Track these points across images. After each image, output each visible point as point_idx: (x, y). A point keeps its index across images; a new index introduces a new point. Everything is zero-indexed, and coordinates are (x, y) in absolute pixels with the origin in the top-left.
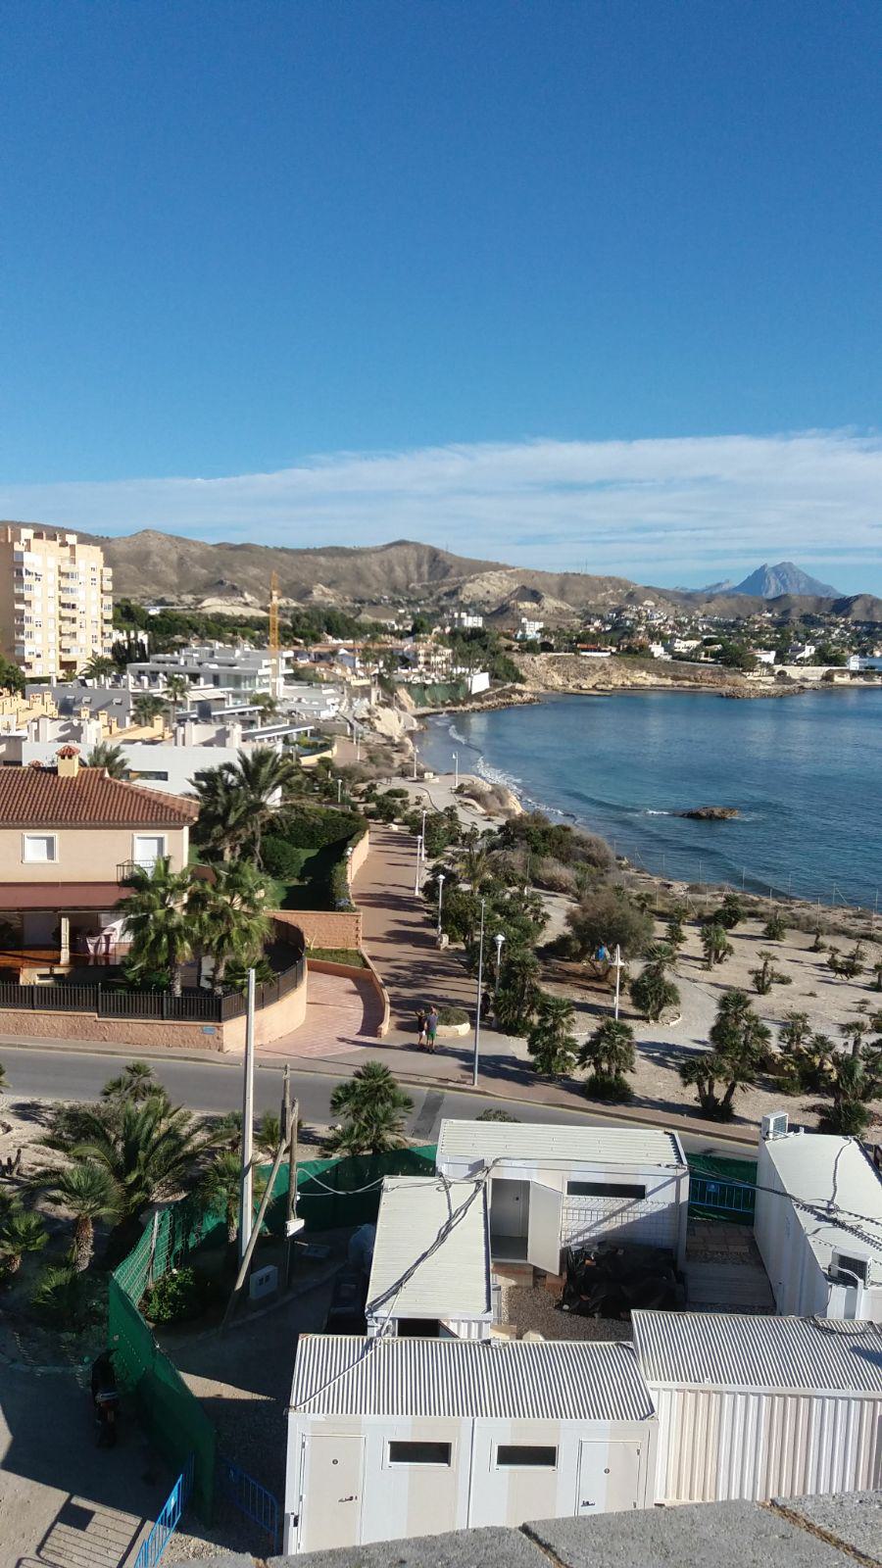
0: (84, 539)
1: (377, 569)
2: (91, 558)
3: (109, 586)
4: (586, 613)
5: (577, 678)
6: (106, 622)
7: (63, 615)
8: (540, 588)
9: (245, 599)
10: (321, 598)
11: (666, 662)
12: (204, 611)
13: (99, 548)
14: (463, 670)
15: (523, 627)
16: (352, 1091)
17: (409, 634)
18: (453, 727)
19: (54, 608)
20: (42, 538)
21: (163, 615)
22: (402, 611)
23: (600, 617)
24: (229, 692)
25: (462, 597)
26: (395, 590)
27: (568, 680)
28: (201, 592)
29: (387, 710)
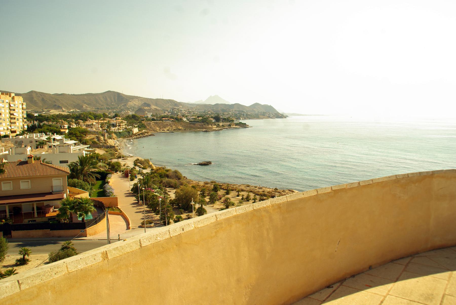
0: (17, 95)
2: (19, 101)
5: (163, 128)
6: (25, 118)
9: (63, 110)
10: (86, 108)
11: (187, 123)
12: (50, 114)
14: (131, 127)
15: (147, 114)
16: (128, 110)
17: (114, 117)
18: (142, 178)
20: (4, 95)
21: (39, 116)
23: (167, 111)
24: (63, 137)
25: (127, 106)
26: (107, 105)
27: (161, 129)
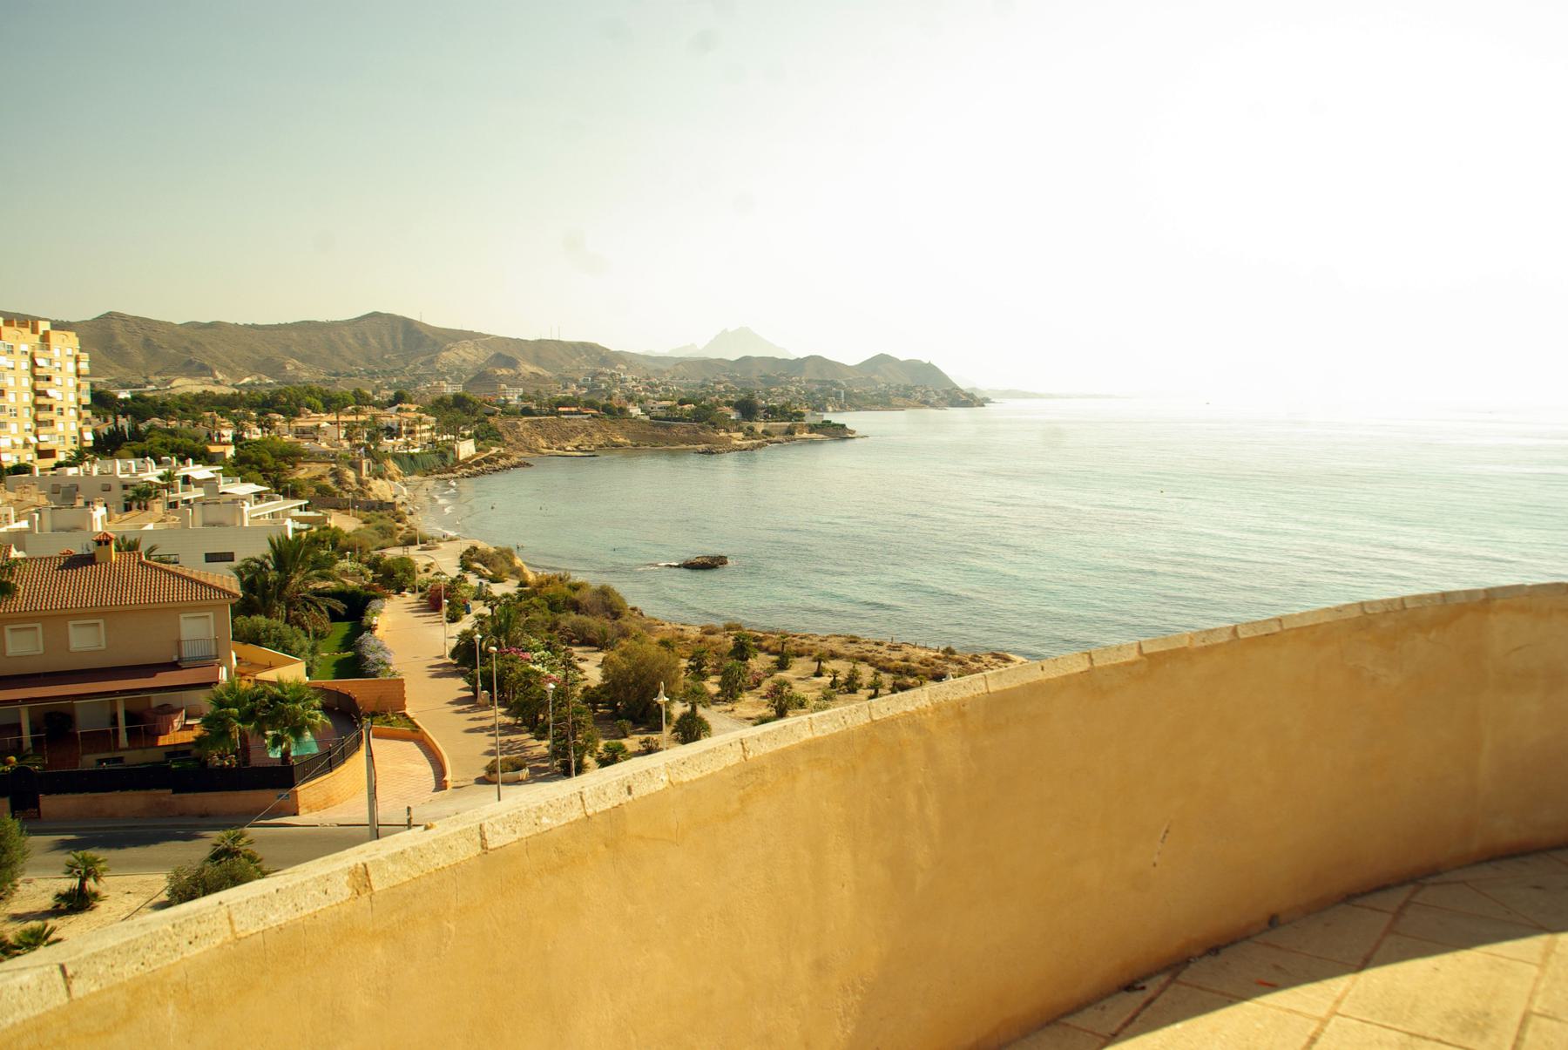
0: (58, 326)
2: (65, 346)
4: (562, 378)
5: (559, 441)
6: (85, 407)
9: (216, 377)
11: (643, 422)
14: (449, 437)
15: (504, 393)
17: (392, 404)
20: (13, 326)
21: (134, 398)
23: (576, 381)
25: (438, 366)
26: (369, 360)
27: (552, 443)
28: (170, 373)
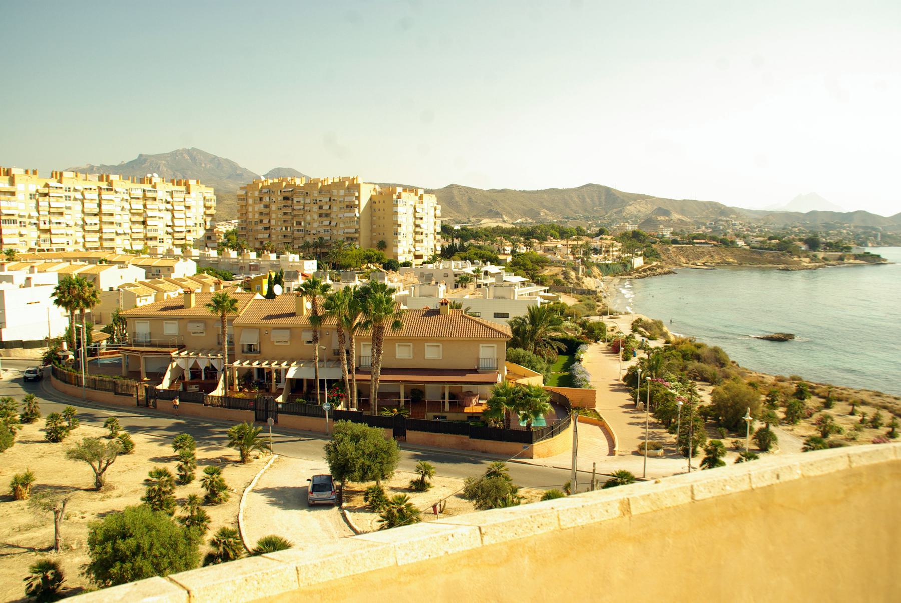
1: (576, 199)
3: (439, 213)
6: (438, 233)
7: (207, 205)
8: (669, 208)
10: (545, 217)
11: (745, 250)
12: (481, 226)
13: (435, 195)
19: (412, 228)
22: (590, 222)
25: (624, 214)
26: (585, 210)
28: (481, 216)
29: (588, 278)
